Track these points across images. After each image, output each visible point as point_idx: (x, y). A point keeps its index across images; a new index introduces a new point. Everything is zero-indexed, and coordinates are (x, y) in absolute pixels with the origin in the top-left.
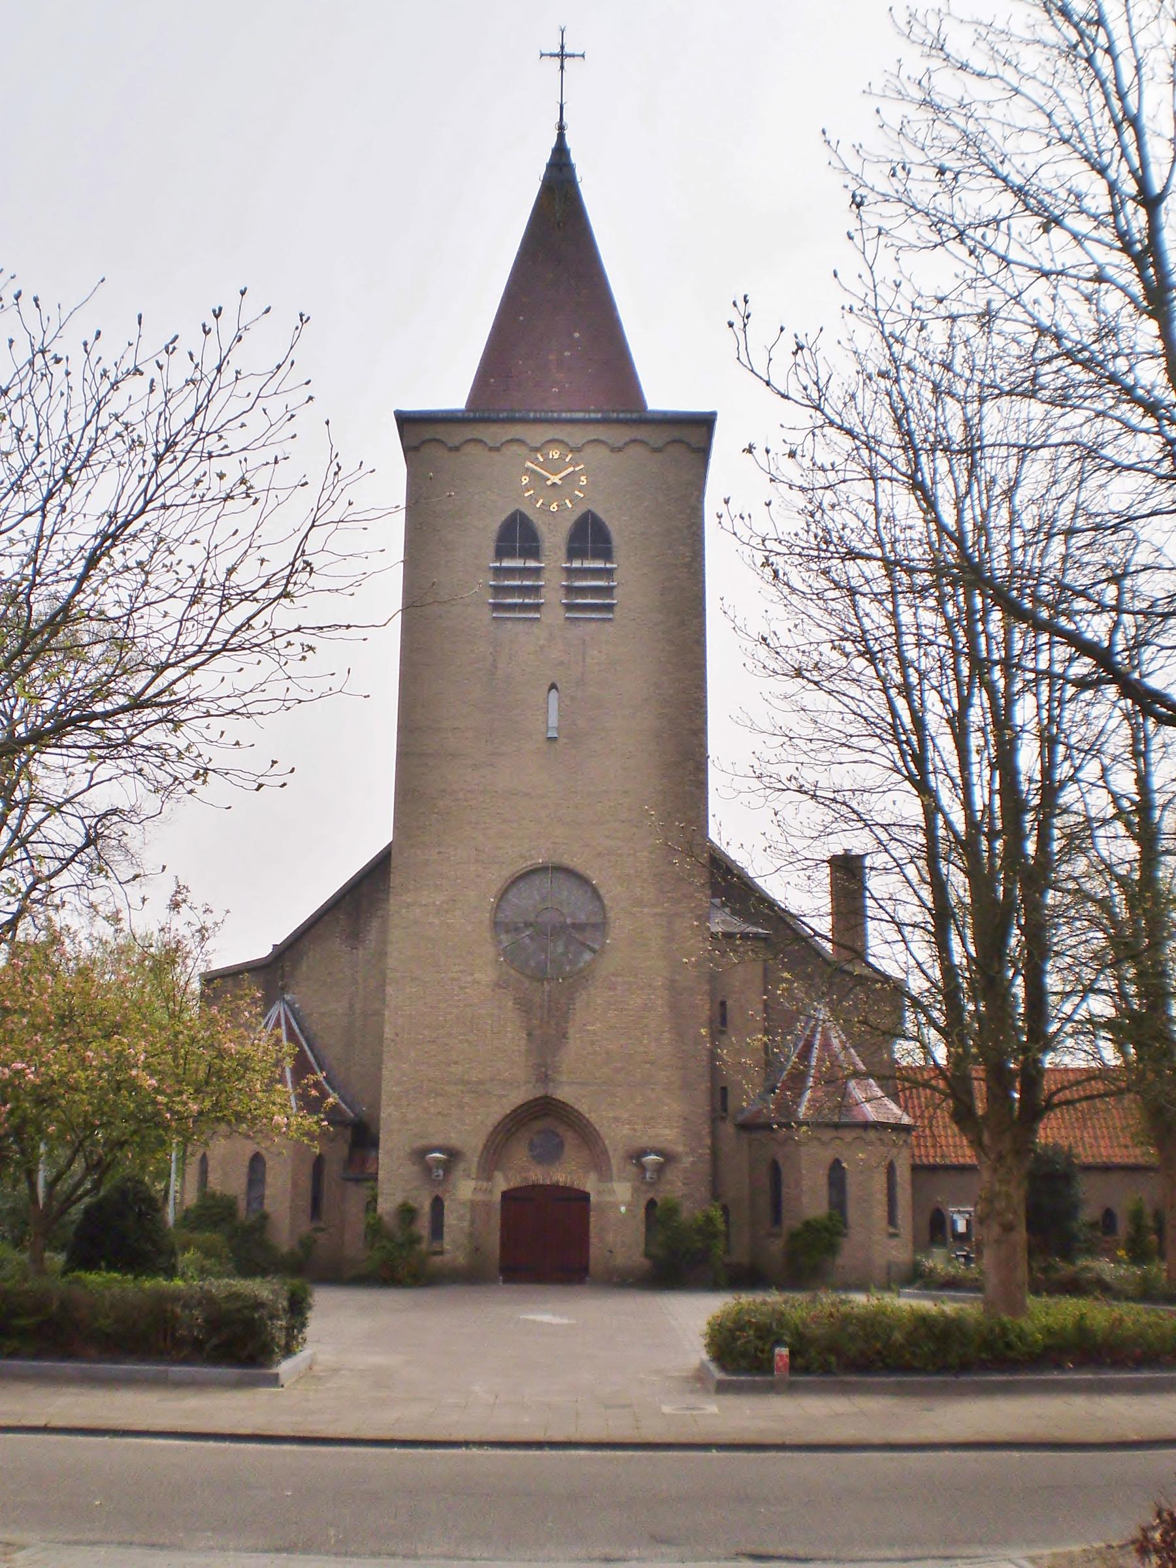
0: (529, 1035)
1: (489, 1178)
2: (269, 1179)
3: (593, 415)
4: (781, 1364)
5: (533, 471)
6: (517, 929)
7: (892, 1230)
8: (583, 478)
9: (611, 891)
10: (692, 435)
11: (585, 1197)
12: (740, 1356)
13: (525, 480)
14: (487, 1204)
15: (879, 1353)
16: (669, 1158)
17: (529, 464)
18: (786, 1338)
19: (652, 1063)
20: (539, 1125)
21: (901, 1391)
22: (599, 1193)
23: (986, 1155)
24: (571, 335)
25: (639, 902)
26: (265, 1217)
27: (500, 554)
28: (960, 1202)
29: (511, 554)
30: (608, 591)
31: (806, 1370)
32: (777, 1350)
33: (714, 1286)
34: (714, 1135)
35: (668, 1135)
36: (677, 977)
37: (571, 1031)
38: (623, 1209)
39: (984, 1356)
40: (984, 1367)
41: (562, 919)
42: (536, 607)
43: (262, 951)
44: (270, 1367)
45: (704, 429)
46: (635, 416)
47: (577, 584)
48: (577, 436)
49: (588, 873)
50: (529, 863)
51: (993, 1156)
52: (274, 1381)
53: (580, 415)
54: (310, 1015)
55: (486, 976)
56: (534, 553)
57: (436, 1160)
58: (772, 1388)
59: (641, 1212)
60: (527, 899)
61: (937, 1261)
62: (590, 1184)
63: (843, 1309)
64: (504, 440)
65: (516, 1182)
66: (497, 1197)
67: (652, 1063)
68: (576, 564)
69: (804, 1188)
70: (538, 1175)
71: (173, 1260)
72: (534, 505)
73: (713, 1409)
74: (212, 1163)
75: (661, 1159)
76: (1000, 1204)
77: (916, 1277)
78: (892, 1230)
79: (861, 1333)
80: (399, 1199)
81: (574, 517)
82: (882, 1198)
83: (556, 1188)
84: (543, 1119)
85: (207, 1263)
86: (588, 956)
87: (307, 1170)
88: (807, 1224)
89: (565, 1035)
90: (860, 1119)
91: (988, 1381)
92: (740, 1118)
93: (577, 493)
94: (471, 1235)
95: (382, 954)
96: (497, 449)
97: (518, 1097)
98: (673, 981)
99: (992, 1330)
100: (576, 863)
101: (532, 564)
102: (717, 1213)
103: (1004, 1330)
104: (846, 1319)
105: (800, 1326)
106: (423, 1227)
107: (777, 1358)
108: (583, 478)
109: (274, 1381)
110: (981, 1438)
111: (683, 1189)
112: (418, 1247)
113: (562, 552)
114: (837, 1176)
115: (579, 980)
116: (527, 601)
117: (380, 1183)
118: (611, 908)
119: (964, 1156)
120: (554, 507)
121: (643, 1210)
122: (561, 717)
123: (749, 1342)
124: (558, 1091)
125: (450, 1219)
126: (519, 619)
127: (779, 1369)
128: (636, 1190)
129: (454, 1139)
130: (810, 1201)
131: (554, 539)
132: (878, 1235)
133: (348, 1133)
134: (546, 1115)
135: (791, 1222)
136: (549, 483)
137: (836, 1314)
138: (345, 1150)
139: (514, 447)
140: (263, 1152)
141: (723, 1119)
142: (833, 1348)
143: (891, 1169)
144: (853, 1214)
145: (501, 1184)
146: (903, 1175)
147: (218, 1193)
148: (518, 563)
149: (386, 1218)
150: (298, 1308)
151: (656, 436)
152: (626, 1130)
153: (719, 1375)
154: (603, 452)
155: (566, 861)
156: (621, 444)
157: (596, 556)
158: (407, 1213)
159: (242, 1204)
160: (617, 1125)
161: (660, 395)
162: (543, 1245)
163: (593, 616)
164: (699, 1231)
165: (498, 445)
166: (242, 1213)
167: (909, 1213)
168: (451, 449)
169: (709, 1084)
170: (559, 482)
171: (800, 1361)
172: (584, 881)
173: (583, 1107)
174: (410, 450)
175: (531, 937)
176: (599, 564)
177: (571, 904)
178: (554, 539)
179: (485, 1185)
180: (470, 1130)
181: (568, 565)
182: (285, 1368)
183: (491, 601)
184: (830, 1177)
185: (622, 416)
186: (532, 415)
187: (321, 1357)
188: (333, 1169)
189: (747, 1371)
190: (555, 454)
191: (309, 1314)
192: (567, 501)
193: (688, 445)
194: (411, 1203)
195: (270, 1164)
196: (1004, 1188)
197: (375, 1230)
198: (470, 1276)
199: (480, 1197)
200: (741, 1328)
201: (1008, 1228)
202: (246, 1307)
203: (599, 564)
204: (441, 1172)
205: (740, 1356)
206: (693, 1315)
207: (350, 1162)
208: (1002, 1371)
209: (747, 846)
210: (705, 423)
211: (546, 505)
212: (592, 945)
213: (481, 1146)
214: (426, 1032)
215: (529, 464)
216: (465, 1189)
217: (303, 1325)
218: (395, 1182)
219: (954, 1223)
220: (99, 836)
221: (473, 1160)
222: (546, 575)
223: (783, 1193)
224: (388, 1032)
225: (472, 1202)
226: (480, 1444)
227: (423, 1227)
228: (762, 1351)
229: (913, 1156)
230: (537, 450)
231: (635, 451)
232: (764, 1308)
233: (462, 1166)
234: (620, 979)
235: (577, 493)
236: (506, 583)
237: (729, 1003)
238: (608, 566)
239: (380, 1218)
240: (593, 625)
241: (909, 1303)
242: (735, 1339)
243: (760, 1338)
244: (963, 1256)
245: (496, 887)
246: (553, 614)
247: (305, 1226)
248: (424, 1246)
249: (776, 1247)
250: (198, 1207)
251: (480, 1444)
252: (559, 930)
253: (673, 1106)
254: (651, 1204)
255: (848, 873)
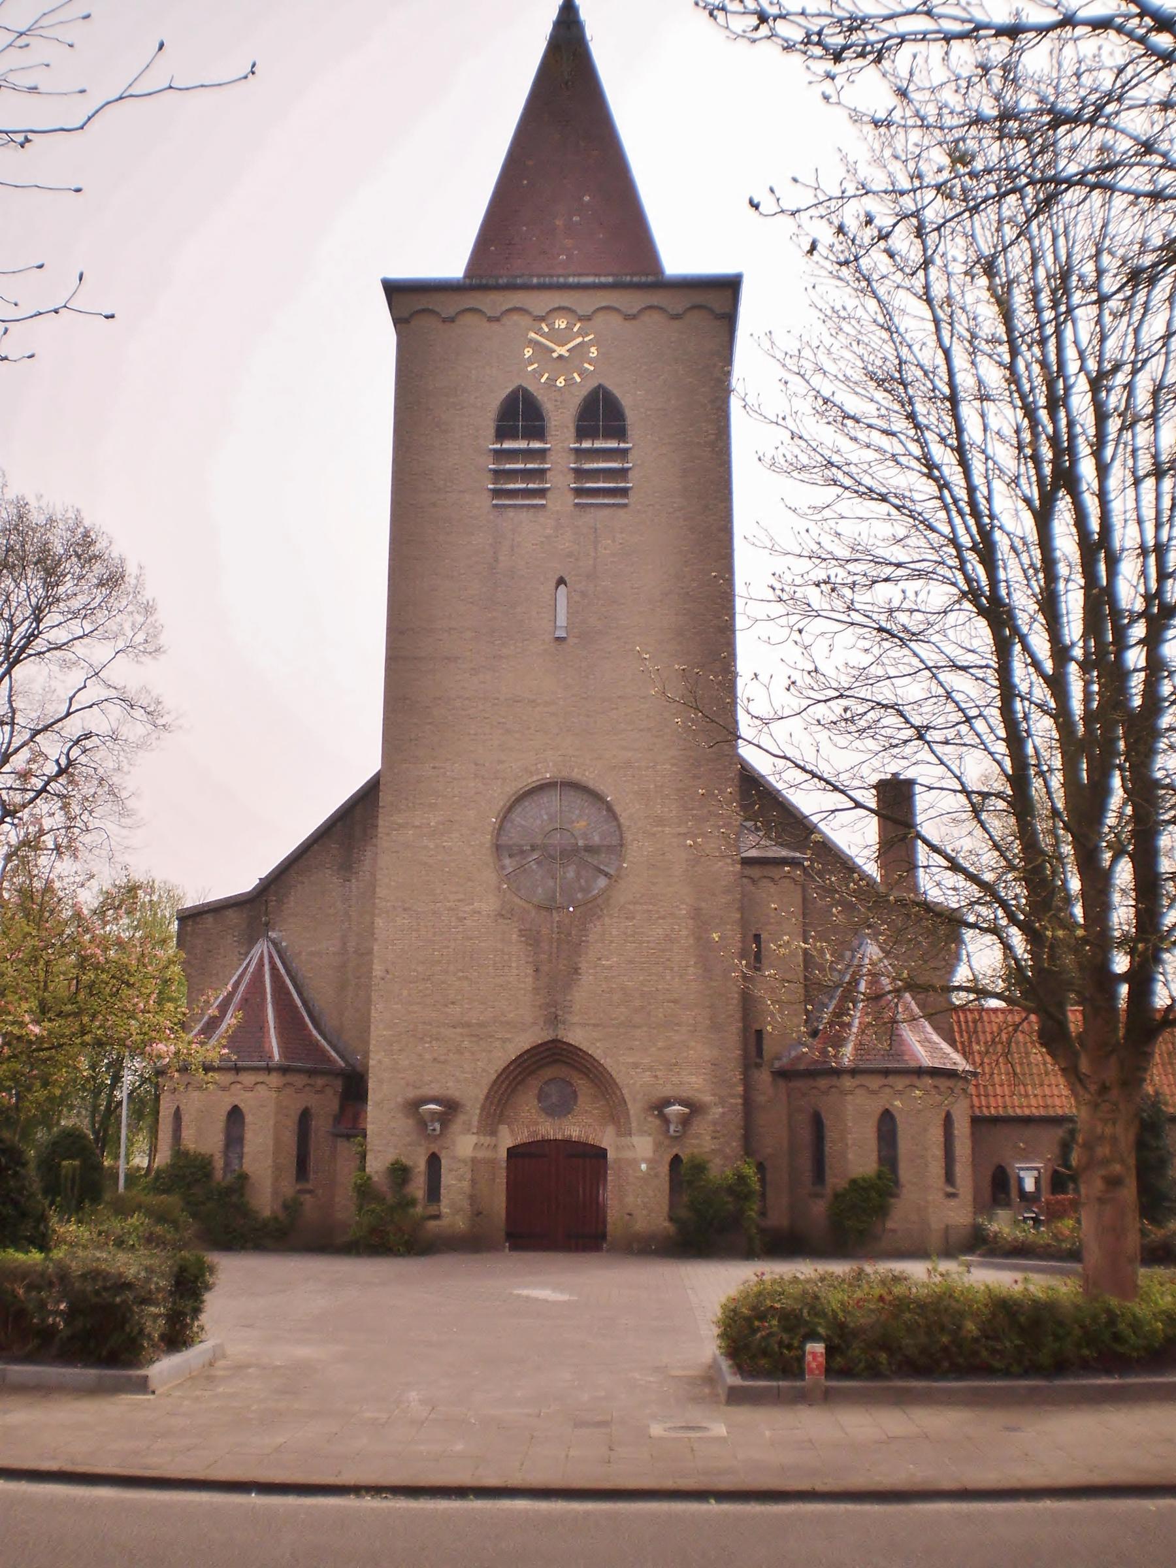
0: (537, 970)
1: (494, 1133)
2: (249, 1135)
3: (603, 280)
4: (814, 1365)
5: (537, 343)
6: (522, 852)
7: (950, 1190)
8: (593, 349)
9: (629, 810)
10: (715, 300)
11: (601, 1153)
12: (763, 1351)
13: (528, 352)
14: (492, 1162)
15: (945, 1349)
16: (695, 1109)
17: (532, 335)
18: (821, 1330)
19: (675, 1002)
20: (549, 1073)
21: (974, 1400)
22: (618, 1148)
23: (1085, 1088)
24: (581, 198)
25: (660, 821)
26: (243, 1178)
27: (502, 433)
28: (1026, 1159)
29: (514, 437)
30: (622, 473)
31: (846, 1373)
32: (809, 1347)
33: (749, 1254)
34: (747, 1083)
35: (694, 1083)
36: (703, 905)
37: (583, 966)
38: (644, 1167)
39: (1086, 1352)
40: (1086, 1367)
41: (573, 841)
42: (542, 493)
43: (245, 883)
44: (138, 1364)
45: (729, 293)
46: (650, 279)
47: (587, 466)
48: (586, 302)
49: (601, 788)
50: (535, 778)
51: (1093, 1088)
52: (143, 1386)
53: (589, 280)
54: (300, 953)
55: (488, 905)
56: (539, 433)
57: (433, 1113)
58: (802, 1398)
59: (664, 1169)
60: (535, 819)
61: (1002, 1224)
62: (606, 1139)
63: (898, 1290)
64: (504, 308)
65: (523, 1137)
66: (503, 1154)
67: (675, 1002)
68: (586, 444)
69: (850, 1142)
70: (549, 1129)
71: (42, 1227)
72: (534, 376)
73: (720, 1429)
74: (186, 1119)
75: (687, 1110)
76: (1103, 1151)
77: (977, 1244)
78: (950, 1190)
79: (921, 1321)
80: (390, 1157)
81: (584, 392)
82: (939, 1152)
83: (568, 1142)
84: (552, 1066)
85: (158, 1229)
86: (602, 882)
87: (291, 1124)
88: (854, 1182)
89: (576, 970)
90: (913, 1064)
91: (1092, 1386)
92: (777, 1064)
93: (586, 365)
94: (472, 1198)
95: (373, 885)
96: (497, 319)
97: (525, 1041)
98: (698, 910)
99: (1095, 1318)
100: (588, 777)
101: (536, 445)
102: (750, 1171)
103: (1112, 1318)
104: (901, 1305)
105: (841, 1315)
106: (418, 1187)
107: (809, 1358)
108: (593, 349)
109: (143, 1386)
110: (1097, 1479)
111: (714, 1145)
112: (411, 1210)
113: (571, 431)
114: (887, 1125)
115: (591, 909)
116: (531, 486)
117: (369, 1139)
118: (629, 827)
119: (1029, 1106)
120: (560, 382)
121: (667, 1167)
122: (570, 614)
123: (770, 1335)
124: (570, 1035)
125: (448, 1179)
126: (523, 506)
127: (811, 1371)
128: (658, 1146)
129: (452, 1090)
130: (856, 1156)
131: (561, 420)
132: (934, 1197)
133: (339, 1084)
134: (556, 1061)
135: (835, 1181)
136: (555, 355)
137: (888, 1298)
138: (335, 1105)
139: (515, 317)
140: (242, 1105)
141: (758, 1066)
142: (886, 1344)
143: (948, 1121)
144: (905, 1172)
145: (507, 1139)
146: (962, 1128)
147: (192, 1152)
148: (521, 444)
149: (375, 1179)
150: (189, 1287)
151: (675, 302)
152: (647, 1077)
153: (735, 1380)
154: (615, 320)
155: (576, 775)
156: (635, 311)
157: (608, 436)
158: (400, 1173)
159: (219, 1163)
160: (636, 1071)
161: (677, 260)
162: (554, 1207)
163: (606, 501)
164: (730, 1190)
165: (498, 314)
166: (218, 1174)
167: (969, 1171)
168: (444, 320)
169: (740, 1025)
170: (567, 354)
171: (839, 1361)
172: (596, 797)
173: (597, 1051)
174: (400, 321)
175: (539, 862)
176: (612, 444)
177: (583, 824)
178: (561, 420)
179: (487, 1140)
180: (470, 1077)
181: (577, 445)
182: (163, 1368)
183: (491, 486)
184: (879, 1130)
185: (636, 279)
186: (535, 280)
187: (231, 1350)
188: (321, 1125)
189: (769, 1375)
190: (561, 324)
191: (207, 1296)
192: (575, 375)
193: (711, 310)
194: (404, 1160)
195: (249, 1119)
196: (1108, 1130)
197: (365, 1190)
198: (471, 1243)
199: (480, 1154)
200: (762, 1317)
201: (1114, 1182)
202: (105, 1289)
203: (612, 444)
204: (437, 1126)
205: (763, 1351)
206: (717, 1286)
207: (338, 1119)
208: (1109, 1372)
209: (764, 678)
210: (730, 286)
211: (552, 380)
212: (606, 869)
213: (482, 1097)
214: (420, 969)
215: (532, 335)
216: (464, 1144)
217: (197, 1311)
218: (386, 1137)
219: (1020, 1181)
220: (70, 763)
221: (473, 1112)
222: (552, 457)
223: (827, 1149)
224: (378, 969)
225: (474, 1160)
226: (377, 1490)
227: (418, 1187)
228: (789, 1347)
229: (972, 1107)
230: (542, 319)
231: (653, 320)
232: (791, 1290)
233: (461, 1118)
234: (638, 907)
235: (586, 365)
236: (508, 466)
237: (764, 936)
238: (622, 445)
239: (369, 1178)
240: (607, 512)
241: (986, 1278)
242: (755, 1331)
243: (786, 1329)
244: (1032, 1218)
245: (501, 803)
246: (561, 501)
247: (289, 1187)
248: (419, 1210)
249: (819, 1208)
250: (172, 1166)
251: (377, 1490)
252: (570, 853)
253: (701, 1051)
254: (676, 1161)
255: (895, 801)
